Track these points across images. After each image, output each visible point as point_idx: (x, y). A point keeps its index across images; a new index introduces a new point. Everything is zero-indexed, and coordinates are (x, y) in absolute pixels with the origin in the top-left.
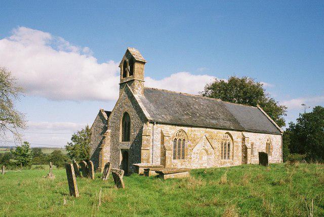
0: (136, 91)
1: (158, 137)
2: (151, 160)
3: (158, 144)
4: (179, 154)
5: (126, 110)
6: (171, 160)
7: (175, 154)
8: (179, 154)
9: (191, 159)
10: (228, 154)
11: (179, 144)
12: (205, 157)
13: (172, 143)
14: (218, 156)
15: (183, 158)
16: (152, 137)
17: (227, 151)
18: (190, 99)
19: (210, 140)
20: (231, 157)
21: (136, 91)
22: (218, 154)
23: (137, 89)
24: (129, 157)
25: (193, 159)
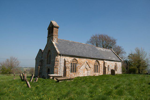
0: (54, 40)
2: (59, 73)
3: (63, 65)
4: (73, 70)
7: (71, 70)
8: (73, 70)
9: (79, 72)
11: (74, 65)
12: (86, 72)
13: (70, 65)
14: (92, 71)
15: (76, 72)
16: (60, 62)
19: (88, 64)
21: (54, 40)
23: (54, 39)
25: (80, 72)
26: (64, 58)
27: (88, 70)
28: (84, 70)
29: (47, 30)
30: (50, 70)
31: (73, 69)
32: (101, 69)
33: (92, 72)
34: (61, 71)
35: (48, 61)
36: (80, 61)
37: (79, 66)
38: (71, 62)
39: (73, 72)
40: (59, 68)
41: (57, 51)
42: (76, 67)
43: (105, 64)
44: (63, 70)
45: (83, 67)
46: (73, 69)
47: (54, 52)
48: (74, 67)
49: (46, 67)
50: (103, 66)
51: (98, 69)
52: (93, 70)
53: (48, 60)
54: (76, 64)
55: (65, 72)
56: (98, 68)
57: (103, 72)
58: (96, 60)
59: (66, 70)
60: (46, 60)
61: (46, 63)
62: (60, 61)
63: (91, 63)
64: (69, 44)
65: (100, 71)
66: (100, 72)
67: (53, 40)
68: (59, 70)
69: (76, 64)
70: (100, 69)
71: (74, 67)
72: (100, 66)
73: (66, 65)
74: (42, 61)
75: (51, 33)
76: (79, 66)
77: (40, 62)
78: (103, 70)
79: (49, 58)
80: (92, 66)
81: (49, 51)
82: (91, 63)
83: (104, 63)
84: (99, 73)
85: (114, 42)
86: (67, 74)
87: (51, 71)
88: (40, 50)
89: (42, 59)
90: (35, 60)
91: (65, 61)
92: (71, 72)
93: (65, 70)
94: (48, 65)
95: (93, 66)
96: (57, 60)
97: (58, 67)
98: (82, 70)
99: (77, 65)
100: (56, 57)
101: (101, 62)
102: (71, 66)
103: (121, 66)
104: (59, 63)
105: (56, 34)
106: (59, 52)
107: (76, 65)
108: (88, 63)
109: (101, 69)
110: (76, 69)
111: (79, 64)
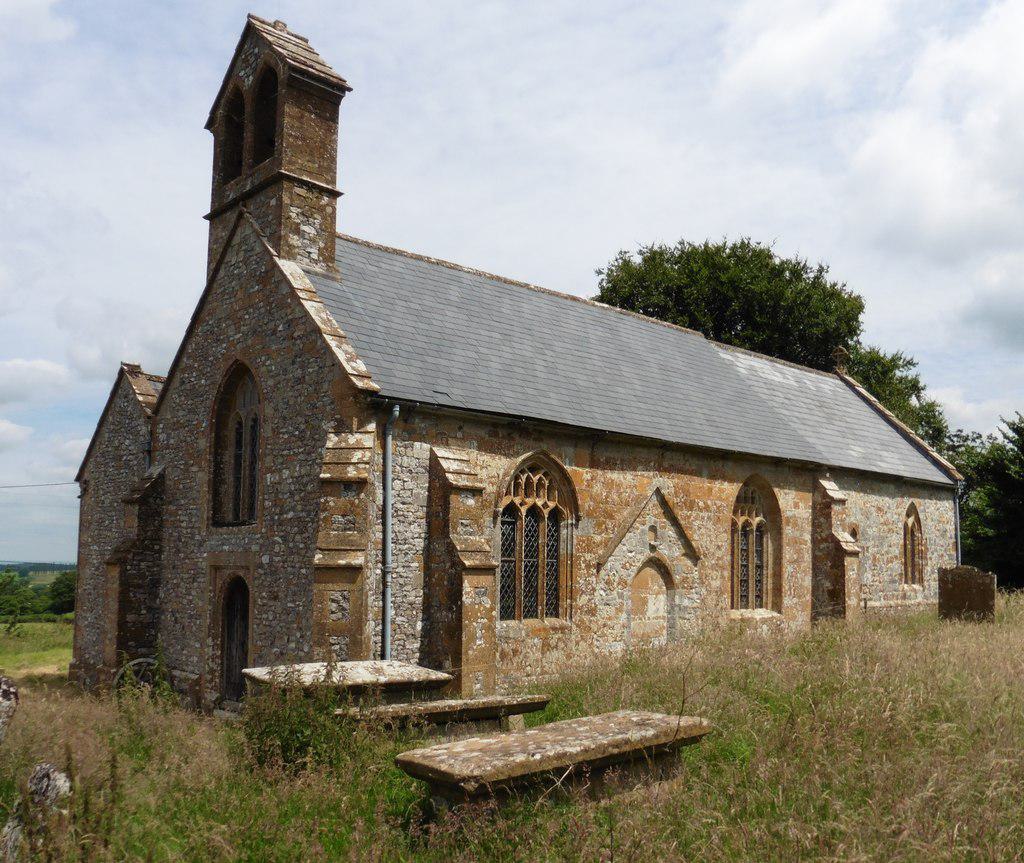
0: (294, 240)
1: (408, 492)
2: (371, 627)
3: (413, 532)
4: (532, 591)
5: (237, 353)
6: (490, 628)
7: (508, 591)
8: (532, 591)
9: (592, 612)
10: (759, 582)
11: (532, 535)
12: (657, 604)
13: (495, 533)
14: (720, 592)
15: (554, 612)
16: (379, 492)
17: (543, 571)
18: (889, 642)
19: (680, 514)
20: (769, 599)
21: (294, 240)
22: (716, 584)
23: (298, 231)
24: (253, 612)
25: (605, 612)
26: (422, 449)
27: (677, 578)
28: (639, 585)
29: (208, 139)
30: (258, 596)
31: (532, 570)
32: (791, 562)
33: (711, 601)
34: (391, 613)
35: (228, 488)
36: (597, 488)
37: (590, 546)
38: (506, 501)
39: (531, 613)
40: (373, 575)
41: (341, 356)
42: (554, 551)
43: (828, 516)
44: (416, 596)
45: (631, 552)
46: (532, 570)
47: (300, 380)
48: (532, 551)
49: (203, 560)
50: (808, 537)
51: (769, 571)
52: (719, 580)
53: (229, 478)
54: (556, 515)
55: (443, 616)
56: (760, 554)
57: (809, 597)
58: (730, 490)
59: (456, 594)
60: (202, 477)
61: (206, 512)
62: (378, 485)
63: (707, 508)
64: (454, 293)
65: (786, 587)
66: (787, 601)
67: (277, 241)
68: (373, 602)
69: (556, 515)
70: (788, 569)
71: (532, 551)
72: (788, 531)
73: (460, 537)
74: (151, 501)
75: (247, 158)
76: (590, 546)
77: (128, 502)
78: (808, 582)
79: (238, 458)
80: (713, 536)
81: (239, 374)
82: (707, 508)
83: (823, 508)
84: (777, 606)
85: (848, 311)
86: (475, 640)
87: (261, 616)
88: (128, 373)
89: (155, 471)
90: (76, 488)
91: (441, 491)
92: (507, 613)
93: (440, 594)
94: (228, 544)
95: (724, 539)
96: (352, 473)
97: (358, 559)
98: (623, 583)
99: (576, 535)
100: (332, 440)
101: (793, 504)
102: (508, 548)
103: (951, 528)
104: (373, 512)
105: (310, 174)
106: (361, 376)
107: (555, 536)
108: (672, 500)
109: (791, 562)
110: (554, 572)
111: (589, 515)
